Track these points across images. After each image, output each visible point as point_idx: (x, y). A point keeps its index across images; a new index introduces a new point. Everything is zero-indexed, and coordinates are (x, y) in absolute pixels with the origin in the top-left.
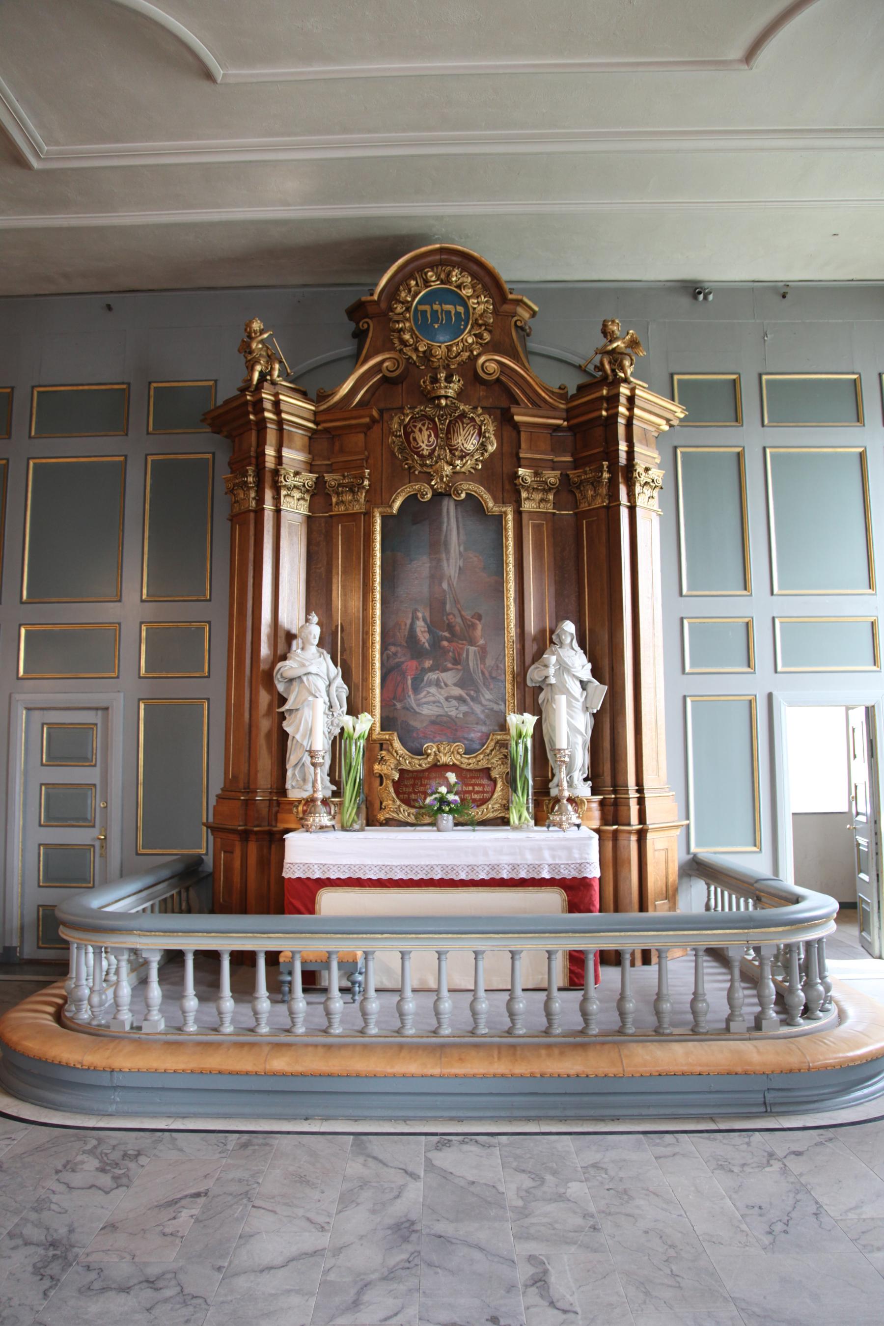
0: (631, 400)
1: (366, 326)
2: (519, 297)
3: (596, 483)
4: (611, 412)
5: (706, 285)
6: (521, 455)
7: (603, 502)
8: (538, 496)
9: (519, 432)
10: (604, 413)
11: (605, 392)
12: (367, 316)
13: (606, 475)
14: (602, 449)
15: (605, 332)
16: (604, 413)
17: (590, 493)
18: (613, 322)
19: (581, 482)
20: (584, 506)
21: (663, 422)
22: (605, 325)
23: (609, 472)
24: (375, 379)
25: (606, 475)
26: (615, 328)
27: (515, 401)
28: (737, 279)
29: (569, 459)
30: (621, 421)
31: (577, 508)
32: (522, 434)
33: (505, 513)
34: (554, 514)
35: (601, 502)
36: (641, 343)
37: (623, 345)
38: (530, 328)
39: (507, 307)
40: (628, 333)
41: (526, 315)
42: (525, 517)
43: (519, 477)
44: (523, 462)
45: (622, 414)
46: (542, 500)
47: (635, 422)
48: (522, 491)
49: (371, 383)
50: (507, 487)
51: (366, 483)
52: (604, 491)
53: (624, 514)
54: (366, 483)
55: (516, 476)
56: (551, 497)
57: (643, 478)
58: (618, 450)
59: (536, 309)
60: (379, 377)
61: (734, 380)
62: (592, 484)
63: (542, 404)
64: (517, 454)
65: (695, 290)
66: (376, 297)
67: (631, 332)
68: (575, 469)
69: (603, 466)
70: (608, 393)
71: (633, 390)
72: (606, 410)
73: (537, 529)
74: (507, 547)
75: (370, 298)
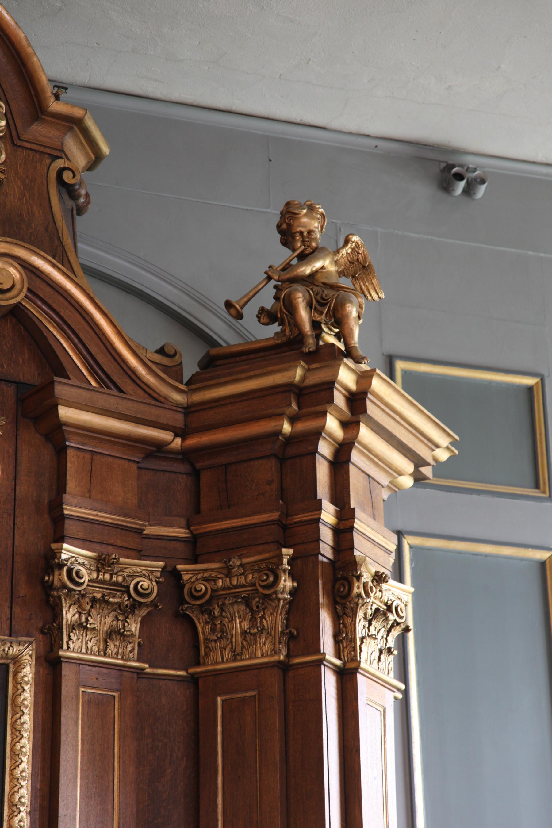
0: (357, 401)
2: (77, 112)
3: (258, 600)
4: (302, 426)
5: (471, 161)
6: (68, 510)
7: (276, 652)
8: (101, 621)
9: (61, 451)
10: (287, 428)
11: (299, 372)
13: (286, 583)
14: (275, 516)
15: (287, 233)
16: (287, 428)
17: (239, 625)
18: (311, 208)
19: (215, 595)
20: (219, 660)
21: (409, 467)
22: (289, 214)
23: (292, 575)
25: (286, 583)
26: (315, 225)
27: (56, 367)
28: (540, 158)
29: (180, 532)
30: (325, 448)
31: (198, 663)
32: (70, 453)
33: (16, 659)
34: (139, 672)
35: (265, 652)
36: (375, 267)
37: (332, 268)
38: (87, 195)
39: (40, 131)
40: (347, 241)
41: (79, 158)
42: (67, 671)
43: (61, 566)
44: (70, 528)
45: (330, 435)
46: (112, 634)
47: (355, 456)
48: (65, 606)
50: (23, 590)
52: (275, 621)
53: (329, 683)
55: (51, 562)
56: (134, 627)
57: (374, 602)
58: (318, 520)
59: (105, 149)
61: (530, 389)
62: (247, 602)
63: (128, 386)
64: (56, 506)
65: (448, 172)
67: (355, 238)
68: (196, 562)
69: (280, 556)
70: (304, 378)
71: (365, 378)
72: (293, 420)
73: (97, 707)
74: (15, 755)
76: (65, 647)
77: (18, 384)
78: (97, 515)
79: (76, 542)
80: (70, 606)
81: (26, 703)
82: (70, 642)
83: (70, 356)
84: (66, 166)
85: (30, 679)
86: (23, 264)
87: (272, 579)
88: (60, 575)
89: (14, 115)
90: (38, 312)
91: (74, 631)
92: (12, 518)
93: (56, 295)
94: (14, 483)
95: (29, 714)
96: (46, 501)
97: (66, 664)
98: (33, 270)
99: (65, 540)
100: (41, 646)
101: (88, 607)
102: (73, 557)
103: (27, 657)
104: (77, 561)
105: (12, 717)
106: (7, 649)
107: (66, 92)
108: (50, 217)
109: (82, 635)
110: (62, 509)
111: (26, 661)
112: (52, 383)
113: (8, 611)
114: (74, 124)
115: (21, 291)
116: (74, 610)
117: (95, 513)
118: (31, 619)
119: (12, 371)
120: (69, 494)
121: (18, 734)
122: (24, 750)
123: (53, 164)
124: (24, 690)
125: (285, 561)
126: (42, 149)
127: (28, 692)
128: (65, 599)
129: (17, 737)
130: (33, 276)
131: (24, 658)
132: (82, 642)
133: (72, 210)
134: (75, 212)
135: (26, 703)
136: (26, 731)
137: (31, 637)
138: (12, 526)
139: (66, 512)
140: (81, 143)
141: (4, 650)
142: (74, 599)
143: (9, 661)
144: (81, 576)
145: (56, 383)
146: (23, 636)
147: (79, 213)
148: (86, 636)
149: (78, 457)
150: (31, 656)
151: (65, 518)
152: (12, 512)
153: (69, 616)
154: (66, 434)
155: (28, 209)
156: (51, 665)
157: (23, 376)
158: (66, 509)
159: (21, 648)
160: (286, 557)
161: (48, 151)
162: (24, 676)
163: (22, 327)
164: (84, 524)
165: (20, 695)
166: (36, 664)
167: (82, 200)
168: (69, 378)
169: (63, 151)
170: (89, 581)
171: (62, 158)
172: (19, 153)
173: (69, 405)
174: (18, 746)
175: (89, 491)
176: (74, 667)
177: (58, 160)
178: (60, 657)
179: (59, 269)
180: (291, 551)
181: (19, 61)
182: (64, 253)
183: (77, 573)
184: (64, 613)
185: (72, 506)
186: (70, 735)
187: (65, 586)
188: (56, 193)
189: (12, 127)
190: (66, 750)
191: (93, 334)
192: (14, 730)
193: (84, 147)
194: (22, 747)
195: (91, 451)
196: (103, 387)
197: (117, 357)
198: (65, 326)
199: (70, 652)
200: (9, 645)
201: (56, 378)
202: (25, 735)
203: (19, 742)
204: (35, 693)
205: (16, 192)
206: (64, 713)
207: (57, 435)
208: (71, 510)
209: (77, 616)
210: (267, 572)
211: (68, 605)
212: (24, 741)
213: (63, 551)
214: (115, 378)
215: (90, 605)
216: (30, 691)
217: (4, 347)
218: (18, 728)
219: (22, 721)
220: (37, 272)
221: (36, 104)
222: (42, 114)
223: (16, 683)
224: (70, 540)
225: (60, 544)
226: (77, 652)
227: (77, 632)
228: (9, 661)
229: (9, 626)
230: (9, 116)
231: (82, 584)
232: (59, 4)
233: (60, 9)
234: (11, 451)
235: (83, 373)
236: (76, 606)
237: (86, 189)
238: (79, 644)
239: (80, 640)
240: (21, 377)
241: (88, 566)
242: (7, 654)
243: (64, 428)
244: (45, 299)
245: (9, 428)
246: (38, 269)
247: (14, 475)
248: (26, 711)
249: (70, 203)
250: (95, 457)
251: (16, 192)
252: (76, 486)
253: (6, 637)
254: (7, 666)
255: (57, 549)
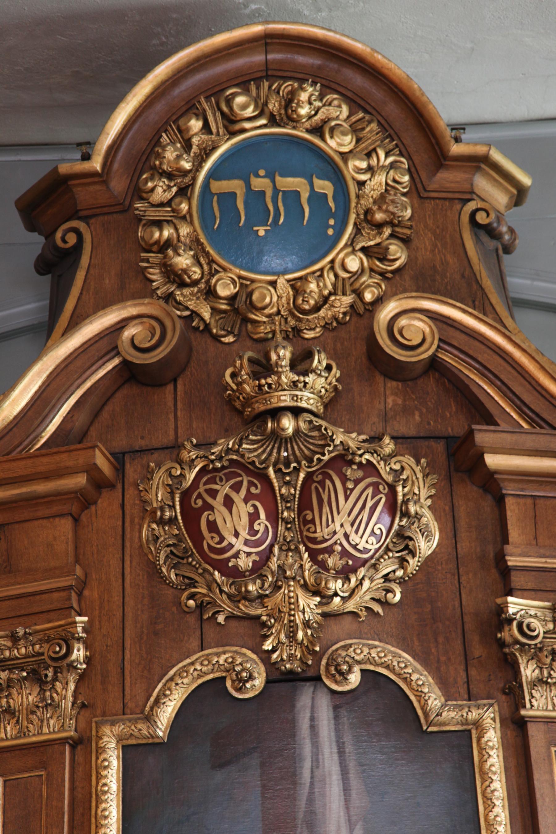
1: (72, 239)
2: (481, 150)
6: (512, 561)
12: (75, 215)
24: (101, 373)
32: (509, 502)
33: (477, 724)
38: (511, 231)
39: (448, 178)
42: (533, 730)
43: (510, 621)
44: (517, 580)
48: (522, 661)
49: (88, 384)
50: (478, 650)
51: (79, 653)
54: (79, 653)
55: (501, 619)
59: (526, 180)
60: (110, 366)
66: (96, 164)
75: (85, 166)
76: (528, 705)
77: (448, 439)
78: (546, 562)
79: (526, 593)
80: (528, 662)
81: (493, 769)
82: (533, 700)
83: (496, 401)
84: (479, 206)
85: (496, 743)
86: (434, 316)
87: (64, 651)
88: (510, 630)
89: (418, 168)
90: (456, 362)
91: (535, 688)
92: (457, 577)
93: (472, 341)
94: (454, 541)
95: (500, 781)
96: (492, 555)
97: (532, 723)
98: (444, 320)
99: (514, 593)
100: (506, 707)
101: (548, 660)
102: (522, 610)
103: (489, 720)
104: (527, 613)
105: (482, 784)
106: (465, 715)
107: (464, 133)
108: (466, 262)
109: (546, 691)
110: (506, 561)
111: (488, 725)
112: (471, 433)
113: (463, 674)
114: (480, 162)
115: (432, 344)
116: (532, 665)
117: (543, 560)
118: (490, 681)
119: (439, 427)
120: (512, 544)
121: (489, 802)
122: (498, 819)
123: (464, 209)
124: (490, 756)
125: (79, 629)
126: (450, 195)
127: (496, 757)
128: (521, 655)
129: (489, 806)
130: (445, 326)
131: (485, 722)
132: (546, 698)
133: (497, 250)
134: (500, 252)
135: (493, 769)
136: (498, 799)
137: (492, 699)
138: (458, 586)
139: (510, 564)
140: (495, 180)
141: (462, 716)
142: (530, 654)
143: (470, 727)
144: (533, 628)
145: (475, 432)
146: (484, 699)
147: (507, 250)
148: (551, 691)
149: (518, 504)
150: (494, 719)
151: (510, 570)
152: (456, 571)
153: (529, 672)
154: (500, 483)
155: (441, 259)
156: (517, 727)
157: (452, 430)
158: (510, 560)
159: (481, 711)
160: (80, 625)
161: (457, 196)
162: (488, 741)
163: (446, 380)
164: (534, 573)
165: (486, 761)
166: (501, 726)
167: (507, 237)
168: (497, 424)
169: (474, 193)
170: (544, 633)
171: (473, 199)
172: (427, 205)
173: (495, 451)
174: (492, 815)
175: (536, 538)
176: (542, 726)
177: (469, 203)
178: (523, 717)
179: (470, 314)
180: (85, 619)
181: (416, 112)
182: (484, 296)
183: (528, 626)
184: (522, 669)
185: (515, 556)
186: (547, 800)
187: (517, 642)
188: (470, 237)
189: (417, 180)
190: (545, 815)
191: (516, 374)
192: (485, 799)
193: (501, 184)
194: (496, 816)
195: (532, 496)
196: (535, 428)
197: (544, 393)
198: (485, 371)
199: (534, 710)
200: (467, 710)
201: (474, 427)
202: (498, 803)
203: (491, 811)
204: (504, 758)
205: (427, 244)
206: (536, 776)
207: (491, 485)
208: (516, 561)
209: (537, 671)
210: (57, 641)
211: (525, 661)
212: (497, 810)
213: (509, 605)
214: (545, 415)
215: (551, 658)
216: (498, 756)
217: (429, 403)
218: (489, 796)
219: (492, 788)
220: (450, 322)
221: (438, 151)
222: (445, 160)
223: (481, 750)
224: (519, 593)
225: (504, 598)
226: (543, 710)
227: (540, 688)
228: (470, 727)
229: (466, 689)
230: (413, 170)
231: (537, 636)
232: (469, 45)
233: (473, 49)
234: (447, 508)
235: (512, 416)
236: (534, 661)
237: (507, 224)
238: (543, 700)
239: (544, 697)
240: (450, 430)
241: (542, 618)
242: (466, 720)
243: (496, 476)
244: (461, 347)
245: (442, 485)
246: (449, 318)
247: (453, 532)
248: (494, 778)
249: (492, 244)
250: (538, 501)
251: (427, 244)
252: (519, 535)
253: (465, 702)
254: (470, 731)
255: (503, 604)
